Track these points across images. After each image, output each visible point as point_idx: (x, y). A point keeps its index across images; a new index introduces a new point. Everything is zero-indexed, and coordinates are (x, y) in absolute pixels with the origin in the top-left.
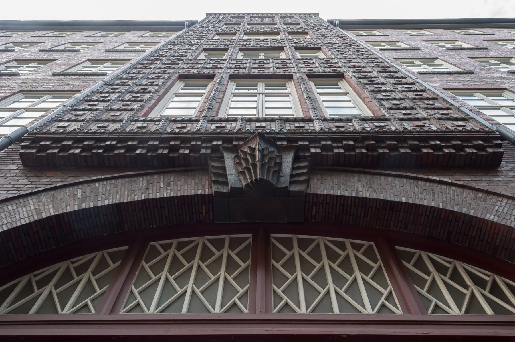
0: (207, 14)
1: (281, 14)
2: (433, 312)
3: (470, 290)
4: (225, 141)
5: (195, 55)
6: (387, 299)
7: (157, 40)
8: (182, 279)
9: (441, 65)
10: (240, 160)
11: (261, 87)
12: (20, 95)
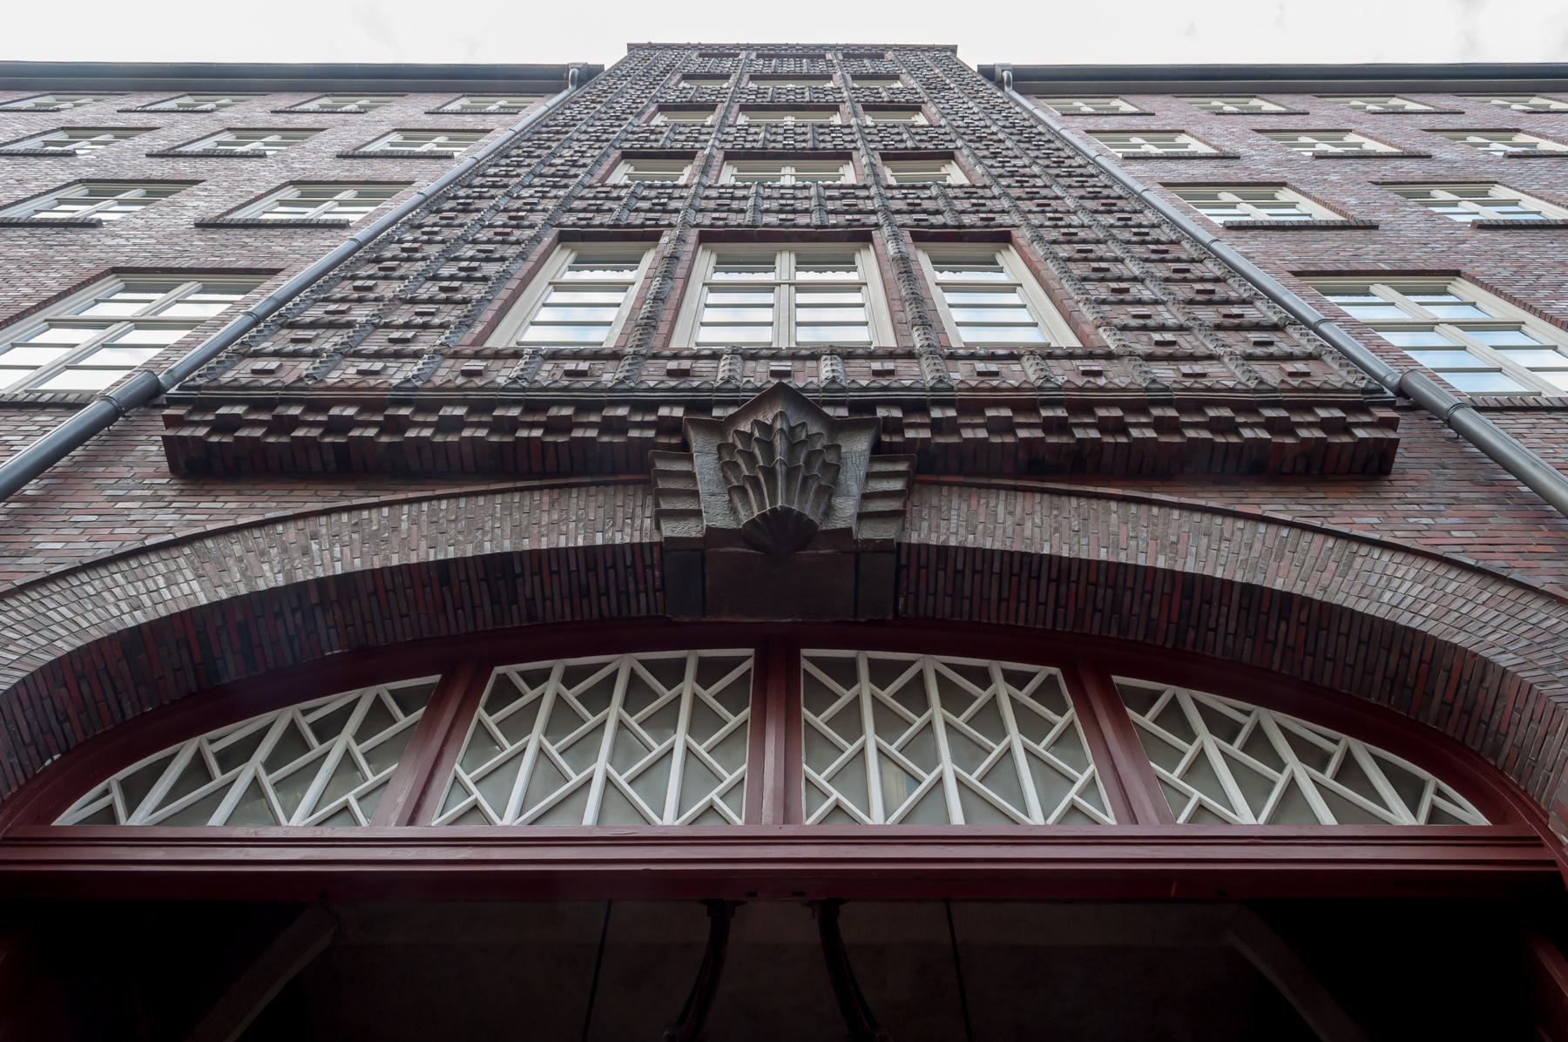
0: (631, 47)
1: (847, 46)
2: (1192, 819)
3: (1287, 772)
4: (690, 406)
5: (600, 172)
6: (1081, 794)
7: (490, 121)
8: (583, 750)
9: (1292, 205)
10: (731, 455)
11: (785, 262)
12: (113, 283)
